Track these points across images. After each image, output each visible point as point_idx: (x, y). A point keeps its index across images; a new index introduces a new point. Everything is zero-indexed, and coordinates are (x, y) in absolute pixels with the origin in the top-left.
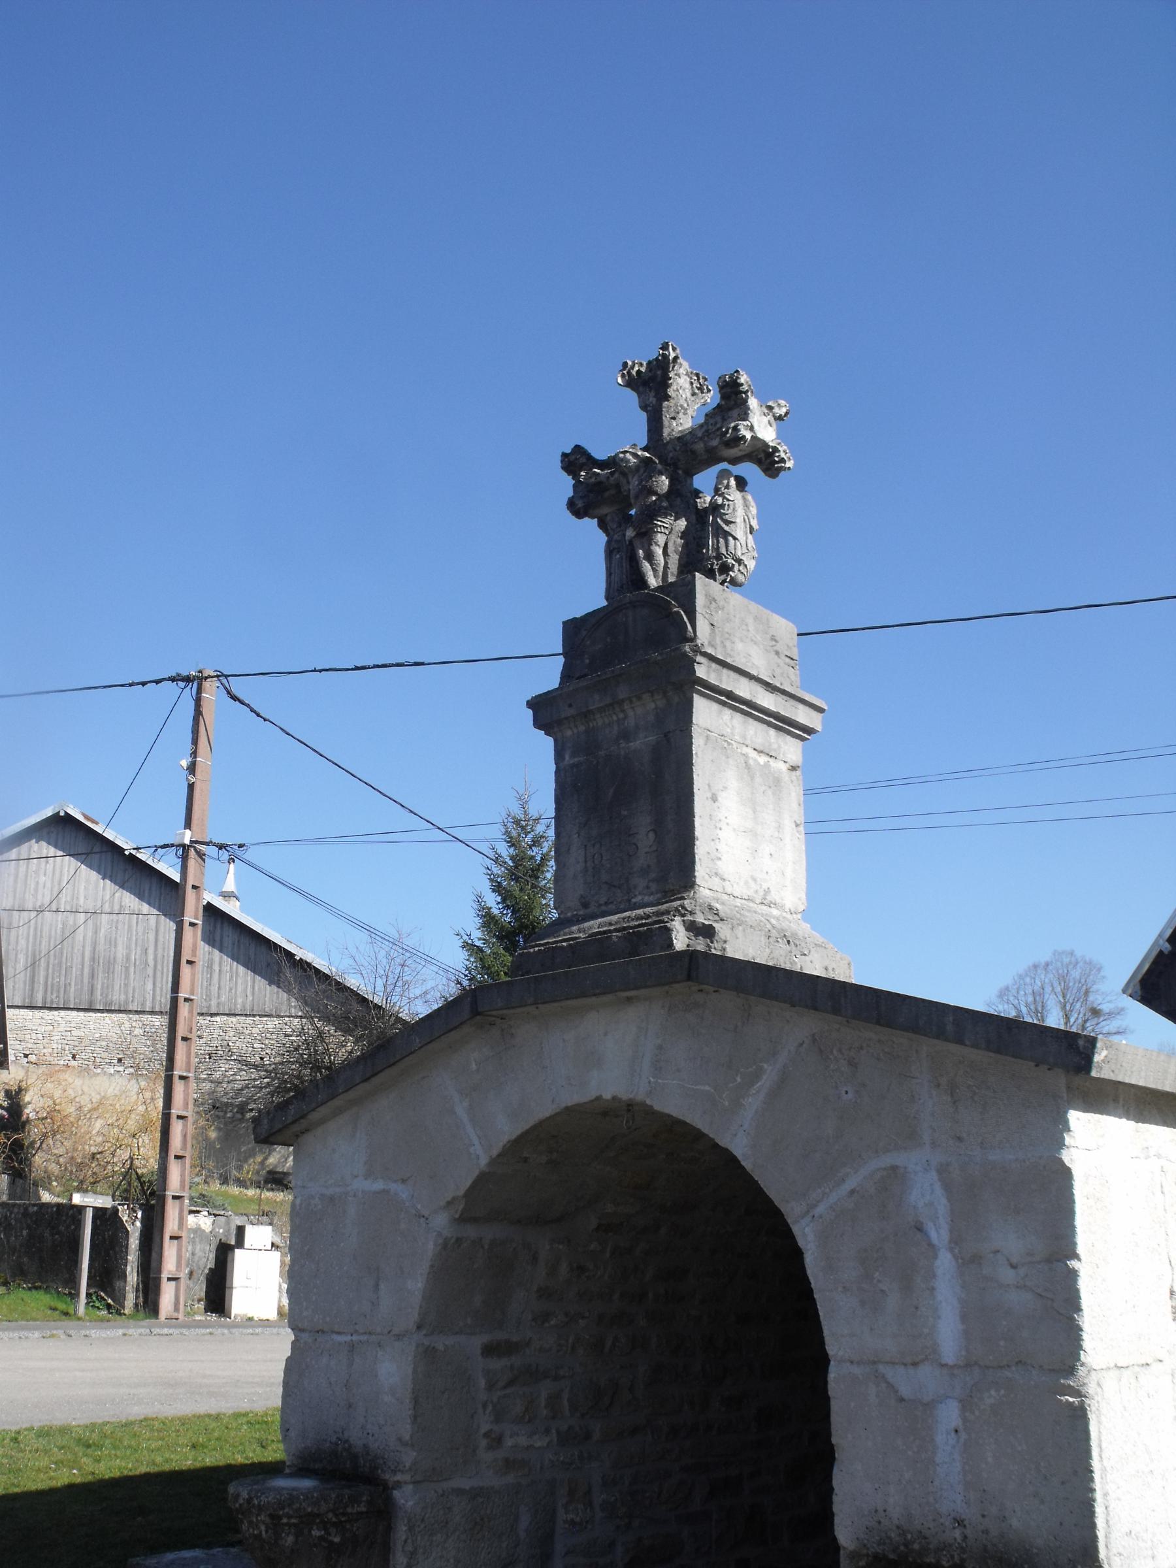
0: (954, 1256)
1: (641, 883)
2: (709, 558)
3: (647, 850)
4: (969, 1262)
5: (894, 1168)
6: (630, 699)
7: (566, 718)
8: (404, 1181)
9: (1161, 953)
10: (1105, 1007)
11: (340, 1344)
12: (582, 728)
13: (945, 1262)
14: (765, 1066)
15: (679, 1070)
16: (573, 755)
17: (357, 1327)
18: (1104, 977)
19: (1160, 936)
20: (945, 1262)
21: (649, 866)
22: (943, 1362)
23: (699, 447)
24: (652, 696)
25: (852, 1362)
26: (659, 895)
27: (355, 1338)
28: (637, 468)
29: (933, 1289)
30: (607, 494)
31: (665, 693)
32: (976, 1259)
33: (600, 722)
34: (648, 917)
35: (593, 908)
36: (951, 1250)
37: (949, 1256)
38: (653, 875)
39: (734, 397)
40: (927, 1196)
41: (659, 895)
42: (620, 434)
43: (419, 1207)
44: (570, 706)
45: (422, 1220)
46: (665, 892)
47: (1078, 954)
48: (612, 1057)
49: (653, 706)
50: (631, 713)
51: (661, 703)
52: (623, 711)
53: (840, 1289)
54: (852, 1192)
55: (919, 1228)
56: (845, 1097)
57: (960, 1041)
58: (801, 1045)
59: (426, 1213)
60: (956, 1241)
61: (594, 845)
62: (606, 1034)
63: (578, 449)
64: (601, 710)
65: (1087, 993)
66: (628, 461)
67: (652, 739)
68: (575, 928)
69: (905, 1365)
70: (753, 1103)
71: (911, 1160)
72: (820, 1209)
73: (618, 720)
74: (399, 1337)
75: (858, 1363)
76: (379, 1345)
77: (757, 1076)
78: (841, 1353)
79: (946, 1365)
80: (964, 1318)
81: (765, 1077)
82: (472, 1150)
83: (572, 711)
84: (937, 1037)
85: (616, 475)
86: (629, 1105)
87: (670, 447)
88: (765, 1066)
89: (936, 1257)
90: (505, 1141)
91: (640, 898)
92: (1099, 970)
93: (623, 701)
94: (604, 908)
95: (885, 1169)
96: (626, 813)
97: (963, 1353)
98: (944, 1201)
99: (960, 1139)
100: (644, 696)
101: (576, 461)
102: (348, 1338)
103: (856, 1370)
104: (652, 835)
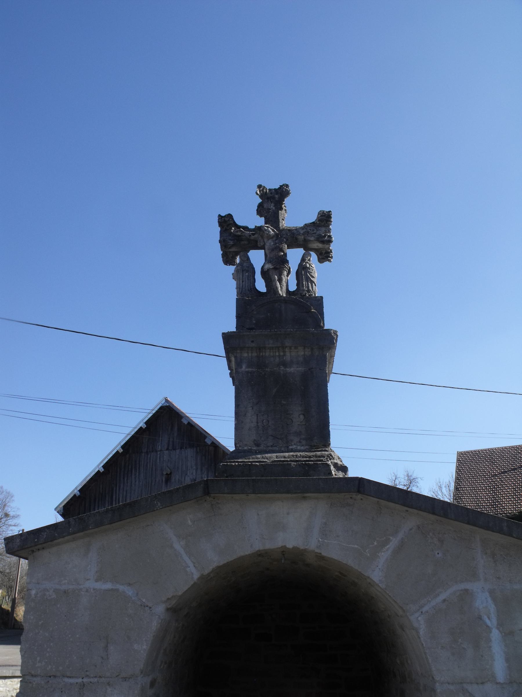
0: (500, 631)
1: (296, 439)
2: (304, 290)
3: (299, 423)
4: (508, 634)
5: (466, 590)
6: (290, 348)
7: (248, 347)
8: (130, 585)
9: (75, 495)
10: (11, 514)
11: (71, 684)
12: (255, 354)
13: (495, 634)
14: (391, 538)
15: (338, 536)
16: (248, 366)
17: (88, 673)
18: (13, 500)
19: (76, 488)
20: (495, 634)
21: (300, 432)
22: (498, 682)
23: (301, 238)
24: (304, 348)
25: (449, 684)
26: (307, 447)
27: (85, 680)
28: (273, 237)
29: (490, 647)
30: (243, 243)
31: (312, 349)
32: (511, 633)
33: (267, 354)
34: (310, 457)
35: (262, 447)
36: (498, 628)
37: (497, 631)
38: (303, 437)
39: (325, 222)
40: (484, 603)
41: (307, 447)
42: (249, 218)
43: (144, 600)
44: (252, 342)
45: (147, 608)
46: (311, 446)
47: (5, 488)
48: (291, 527)
49: (302, 353)
50: (288, 354)
51: (308, 352)
52: (284, 352)
53: (440, 648)
54: (444, 601)
55: (480, 618)
56: (437, 556)
57: (510, 535)
58: (411, 529)
59: (150, 605)
60: (500, 625)
61: (263, 415)
62: (288, 514)
63: (230, 216)
64: (271, 348)
65: (5, 505)
66: (269, 232)
67: (301, 369)
68: (259, 456)
69: (477, 684)
70: (384, 555)
71: (474, 587)
72: (425, 609)
73: (279, 356)
74: (125, 679)
75: (452, 684)
76: (109, 684)
77: (387, 541)
78: (442, 679)
79: (499, 683)
80: (507, 660)
81: (391, 543)
82: (188, 569)
83: (253, 345)
84: (499, 532)
85: (256, 236)
86: (283, 551)
87: (284, 232)
88: (391, 538)
89: (491, 632)
90: (214, 566)
91: (294, 446)
92: (12, 497)
93: (286, 347)
94: (270, 448)
95: (461, 590)
96: (285, 402)
97: (508, 677)
98: (493, 606)
99: (499, 578)
100: (299, 348)
101: (226, 222)
102: (80, 680)
103: (452, 687)
104: (302, 417)
